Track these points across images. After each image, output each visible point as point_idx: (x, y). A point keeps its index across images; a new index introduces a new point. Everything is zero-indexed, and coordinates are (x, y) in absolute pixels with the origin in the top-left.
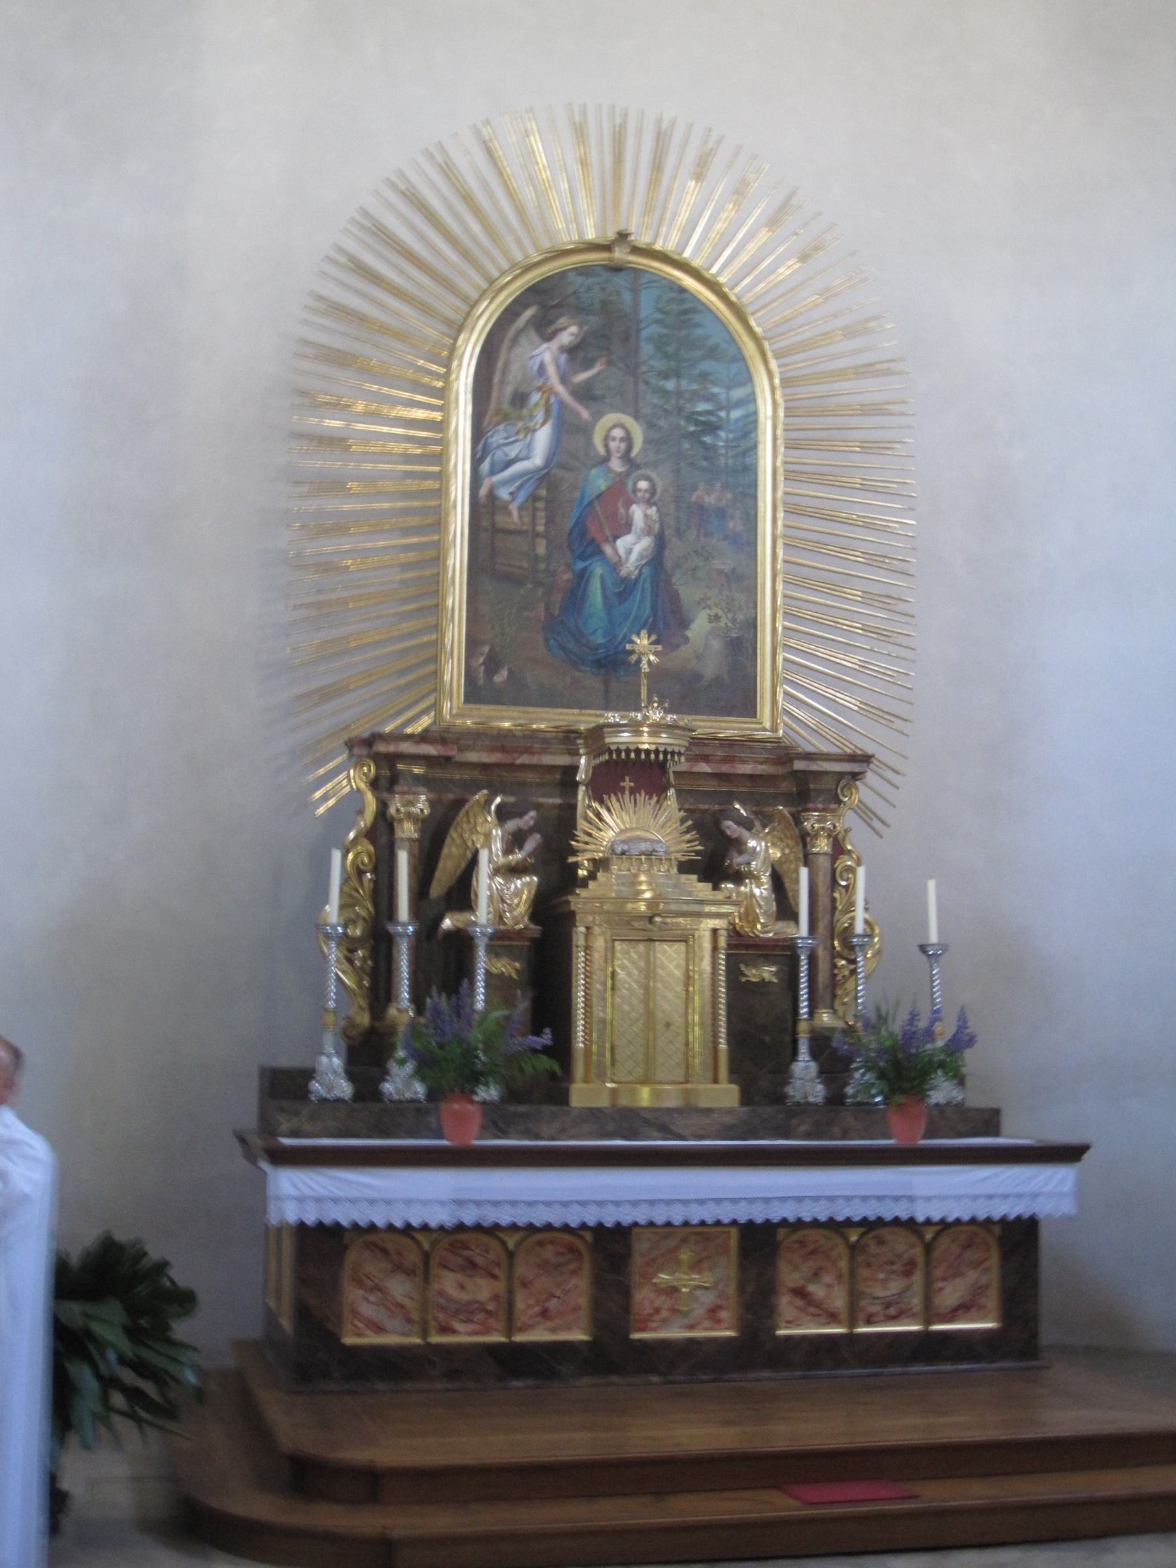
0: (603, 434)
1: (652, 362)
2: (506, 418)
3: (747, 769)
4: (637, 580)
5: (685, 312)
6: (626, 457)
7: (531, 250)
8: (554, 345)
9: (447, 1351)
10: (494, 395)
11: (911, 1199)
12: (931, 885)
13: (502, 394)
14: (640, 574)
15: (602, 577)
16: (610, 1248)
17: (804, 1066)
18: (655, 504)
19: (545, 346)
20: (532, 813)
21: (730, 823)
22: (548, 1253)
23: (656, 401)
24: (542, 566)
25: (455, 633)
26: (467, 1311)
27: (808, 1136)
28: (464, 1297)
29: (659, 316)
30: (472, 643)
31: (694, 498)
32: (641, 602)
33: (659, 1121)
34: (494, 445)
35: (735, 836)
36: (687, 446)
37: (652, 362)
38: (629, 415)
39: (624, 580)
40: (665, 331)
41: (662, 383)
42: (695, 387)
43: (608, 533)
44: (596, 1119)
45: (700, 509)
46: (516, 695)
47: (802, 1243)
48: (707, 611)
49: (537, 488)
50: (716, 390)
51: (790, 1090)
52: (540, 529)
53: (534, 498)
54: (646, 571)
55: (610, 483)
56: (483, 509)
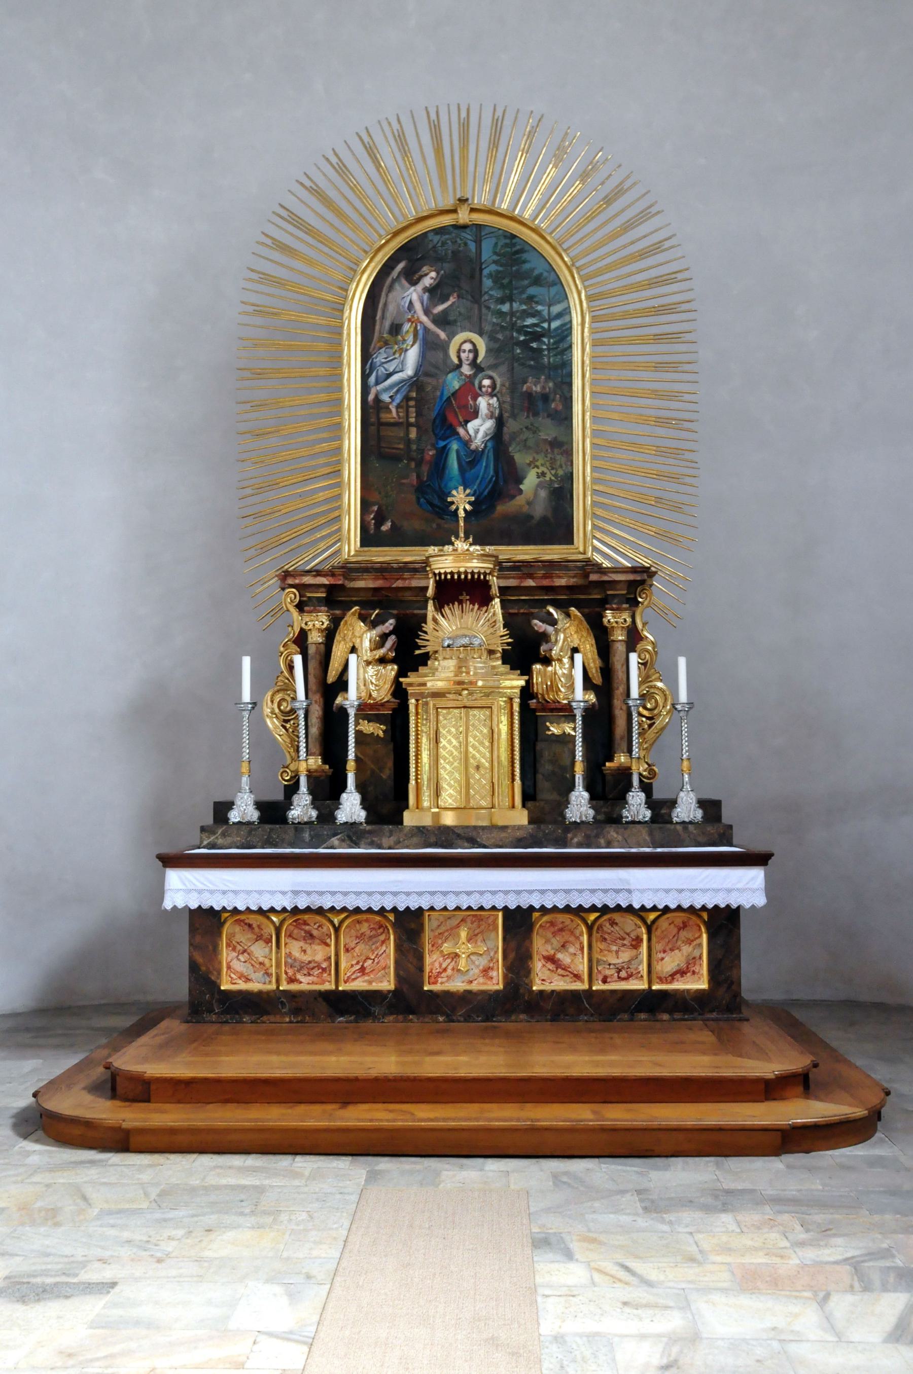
0: (457, 347)
1: (491, 293)
2: (386, 343)
3: (562, 582)
4: (483, 450)
5: (517, 252)
6: (473, 363)
7: (401, 219)
8: (419, 287)
9: (292, 996)
10: (377, 327)
11: (629, 891)
13: (382, 327)
14: (485, 446)
15: (458, 452)
16: (408, 924)
18: (495, 395)
19: (413, 288)
20: (392, 621)
21: (536, 621)
22: (365, 928)
23: (495, 320)
24: (414, 447)
26: (308, 968)
27: (579, 846)
28: (306, 958)
29: (495, 258)
30: (365, 505)
31: (525, 388)
32: (486, 467)
33: (468, 835)
34: (378, 364)
35: (541, 630)
36: (518, 351)
37: (491, 293)
38: (475, 332)
39: (475, 452)
40: (501, 269)
41: (499, 307)
42: (524, 307)
43: (461, 419)
44: (423, 834)
45: (529, 395)
46: (397, 539)
47: (552, 924)
48: (536, 470)
49: (409, 391)
50: (539, 308)
51: (625, 813)
52: (412, 420)
53: (407, 398)
54: (489, 445)
55: (462, 383)
56: (371, 410)
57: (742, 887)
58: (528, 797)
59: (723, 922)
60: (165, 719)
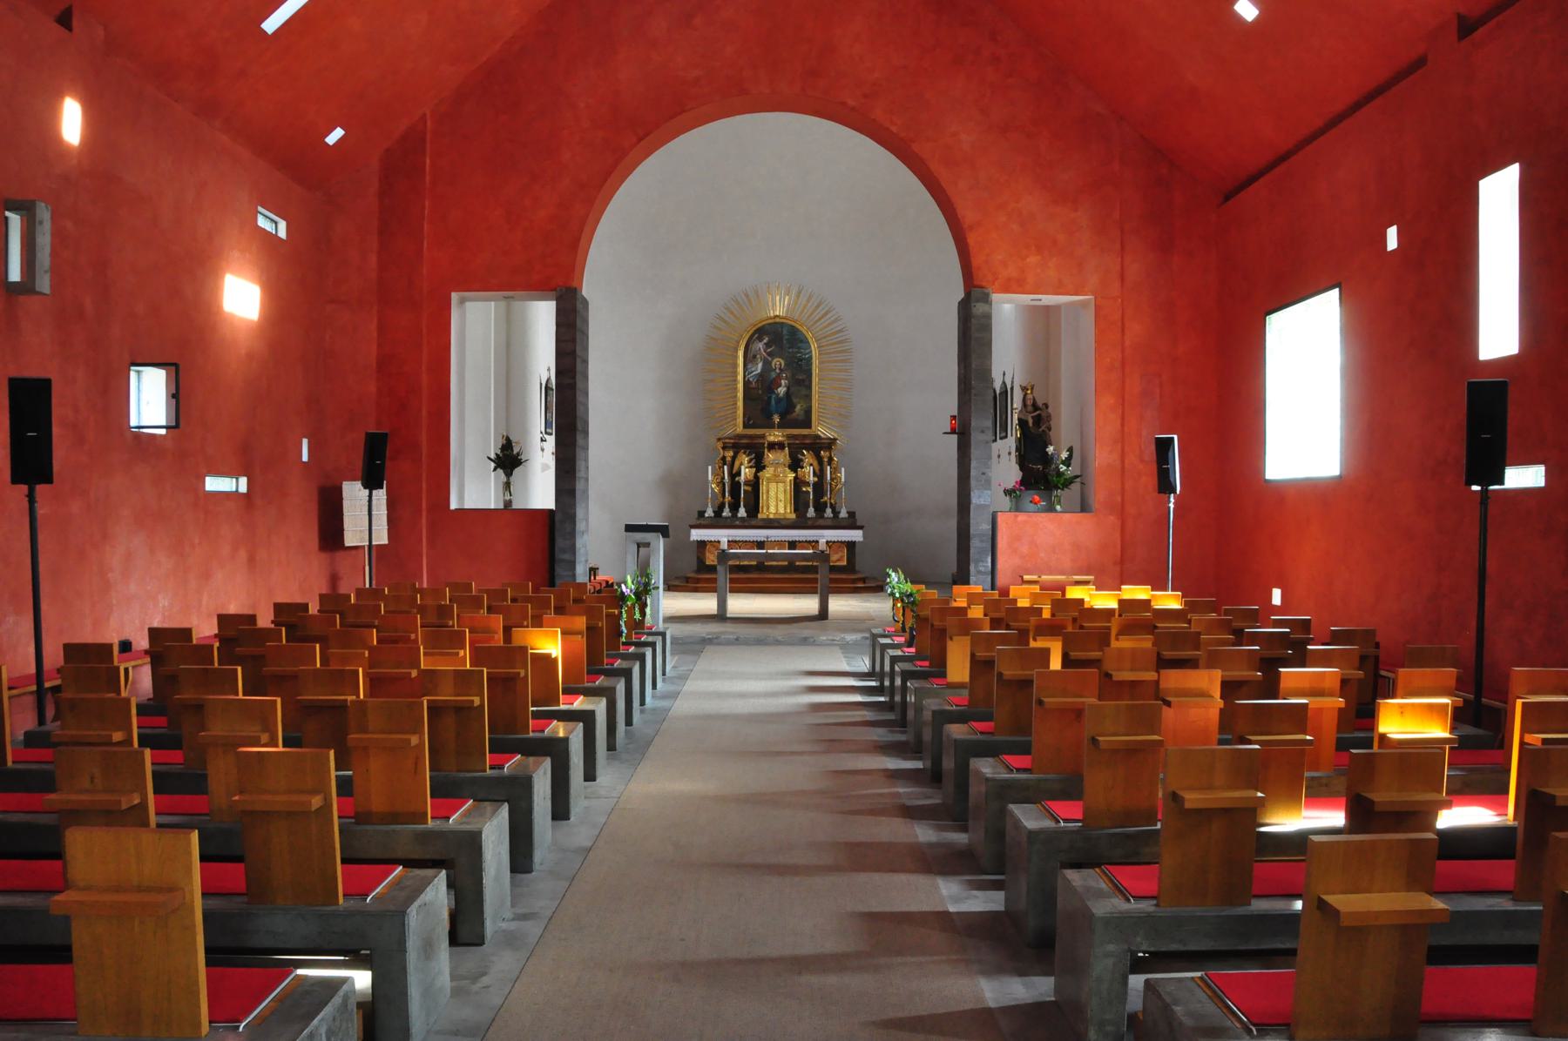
12: (305, 458)
13: (750, 355)
17: (829, 511)
25: (740, 412)
46: (754, 426)
56: (746, 383)
57: (855, 535)
58: (796, 510)
59: (851, 545)
60: (672, 484)
